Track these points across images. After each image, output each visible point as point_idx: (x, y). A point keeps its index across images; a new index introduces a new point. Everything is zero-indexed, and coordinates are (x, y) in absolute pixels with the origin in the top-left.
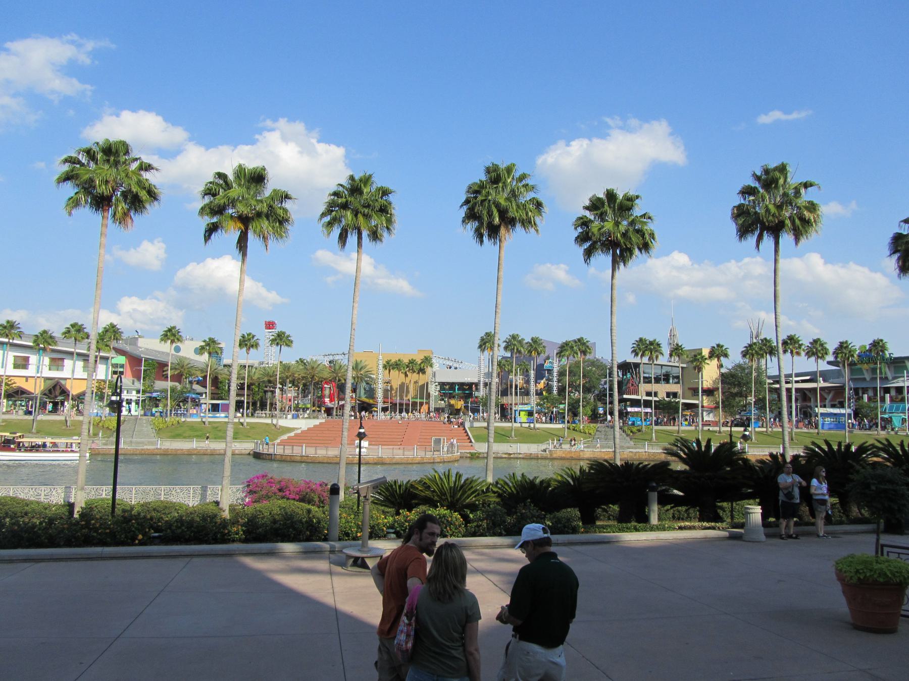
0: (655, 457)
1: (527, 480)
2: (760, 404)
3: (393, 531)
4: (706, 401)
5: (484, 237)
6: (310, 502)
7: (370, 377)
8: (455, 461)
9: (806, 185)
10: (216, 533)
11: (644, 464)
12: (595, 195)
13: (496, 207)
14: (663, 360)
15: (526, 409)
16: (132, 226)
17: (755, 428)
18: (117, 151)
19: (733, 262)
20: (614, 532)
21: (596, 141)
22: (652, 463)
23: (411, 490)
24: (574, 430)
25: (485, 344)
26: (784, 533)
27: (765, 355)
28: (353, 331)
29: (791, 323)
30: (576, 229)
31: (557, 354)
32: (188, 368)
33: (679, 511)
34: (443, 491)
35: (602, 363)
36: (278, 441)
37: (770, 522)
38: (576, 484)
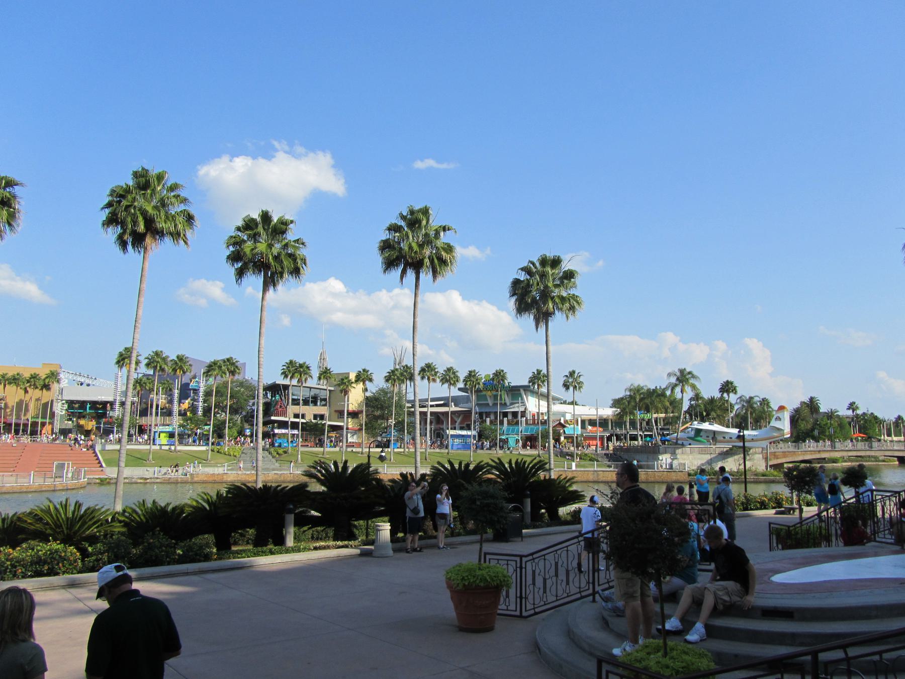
1: (159, 508)
2: (400, 426)
4: (351, 423)
8: (81, 488)
9: (444, 229)
11: (282, 486)
12: (249, 215)
13: (142, 214)
14: (312, 382)
15: (167, 430)
17: (394, 449)
19: (384, 291)
20: (248, 557)
21: (261, 161)
22: (291, 485)
23: (18, 523)
24: (218, 452)
25: (123, 359)
26: (409, 547)
27: (405, 380)
29: (431, 352)
30: (228, 247)
31: (204, 373)
33: (317, 532)
34: (58, 523)
37: (399, 537)
38: (212, 508)
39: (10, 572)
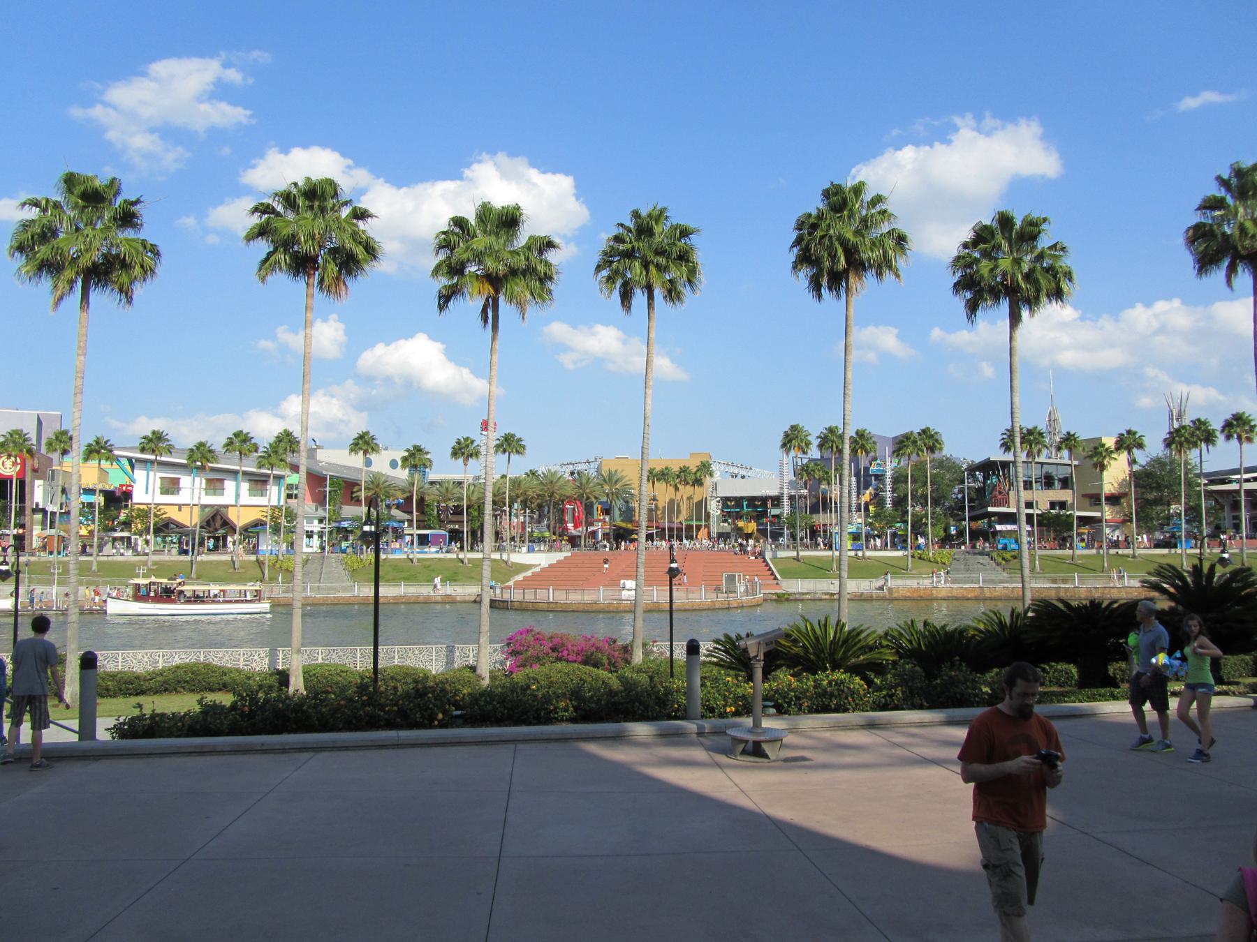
0: (1042, 594)
3: (771, 704)
4: (1108, 513)
5: (823, 289)
6: (596, 665)
7: (630, 493)
10: (538, 709)
13: (841, 244)
16: (346, 294)
18: (323, 193)
20: (1080, 701)
24: (920, 558)
25: (790, 441)
28: (647, 428)
32: (385, 488)
35: (954, 463)
36: (511, 583)
39: (795, 704)
